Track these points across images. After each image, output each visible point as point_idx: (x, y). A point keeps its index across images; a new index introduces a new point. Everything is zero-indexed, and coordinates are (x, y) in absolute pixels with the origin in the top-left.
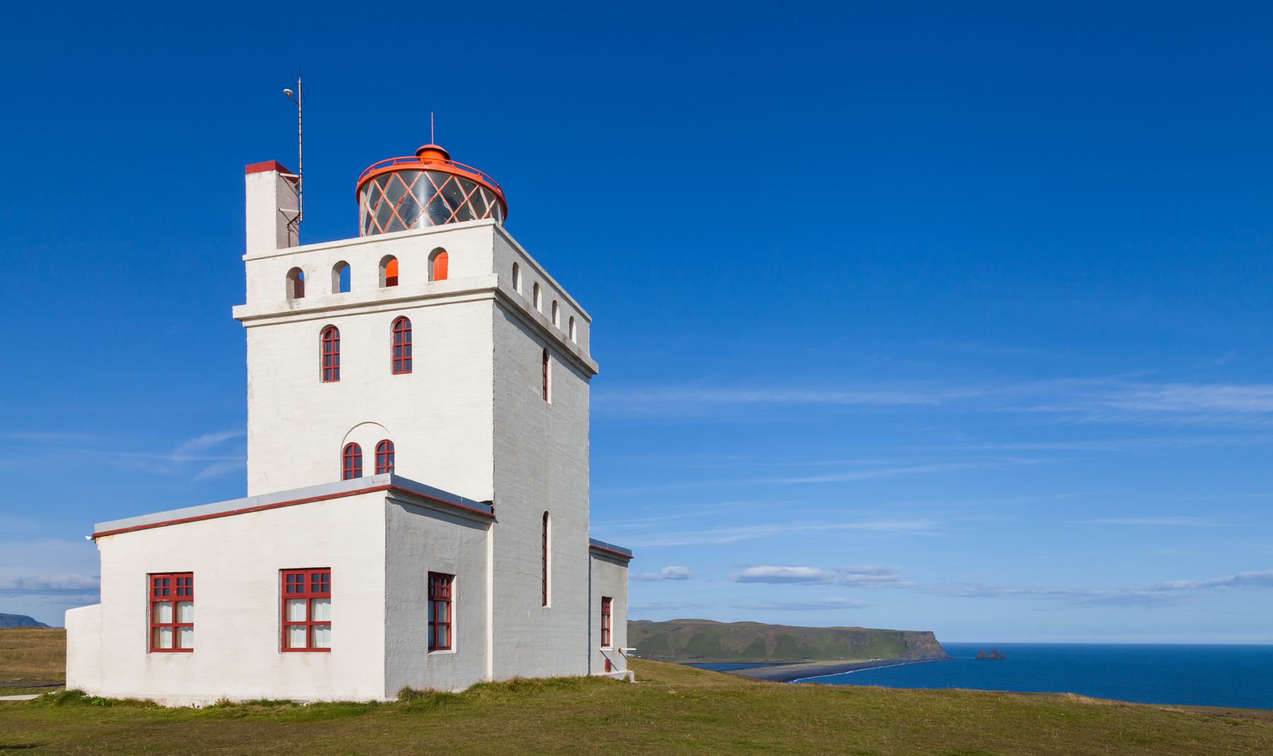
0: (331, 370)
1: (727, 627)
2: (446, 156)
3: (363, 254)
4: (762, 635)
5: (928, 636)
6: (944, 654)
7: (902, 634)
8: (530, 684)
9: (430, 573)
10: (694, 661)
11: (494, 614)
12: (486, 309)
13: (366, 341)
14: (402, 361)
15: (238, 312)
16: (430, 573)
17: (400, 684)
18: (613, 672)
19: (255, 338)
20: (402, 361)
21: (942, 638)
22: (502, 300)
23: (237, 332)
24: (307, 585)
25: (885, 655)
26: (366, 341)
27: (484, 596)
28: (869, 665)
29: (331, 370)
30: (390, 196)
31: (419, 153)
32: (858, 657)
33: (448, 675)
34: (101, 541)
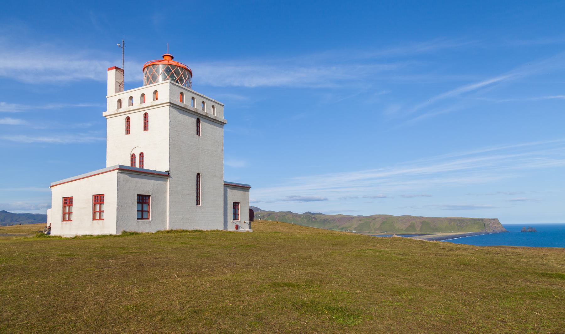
0: (128, 131)
1: (398, 218)
2: (172, 58)
3: (136, 93)
4: (414, 221)
5: (495, 221)
6: (504, 229)
7: (482, 220)
8: (186, 231)
9: (138, 195)
10: (383, 234)
11: (169, 208)
12: (167, 109)
13: (137, 120)
14: (146, 127)
15: (104, 114)
16: (138, 195)
17: (122, 230)
18: (241, 230)
19: (109, 121)
20: (146, 127)
21: (503, 222)
22: (172, 105)
23: (104, 119)
24: (99, 199)
25: (474, 230)
26: (137, 120)
27: (166, 202)
28: (466, 235)
29: (128, 131)
30: (149, 73)
31: (163, 57)
32: (461, 231)
33: (146, 227)
34: (52, 188)
